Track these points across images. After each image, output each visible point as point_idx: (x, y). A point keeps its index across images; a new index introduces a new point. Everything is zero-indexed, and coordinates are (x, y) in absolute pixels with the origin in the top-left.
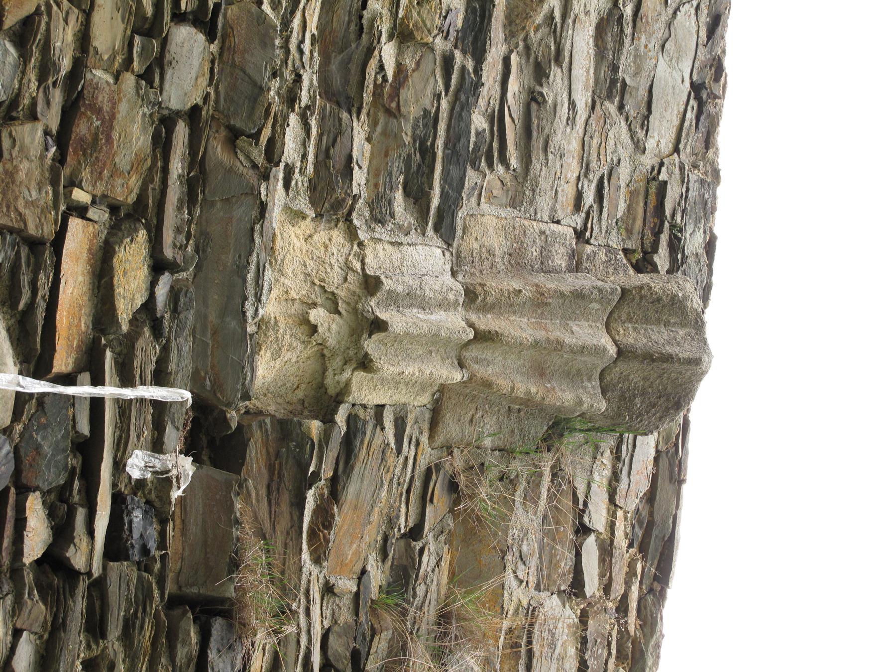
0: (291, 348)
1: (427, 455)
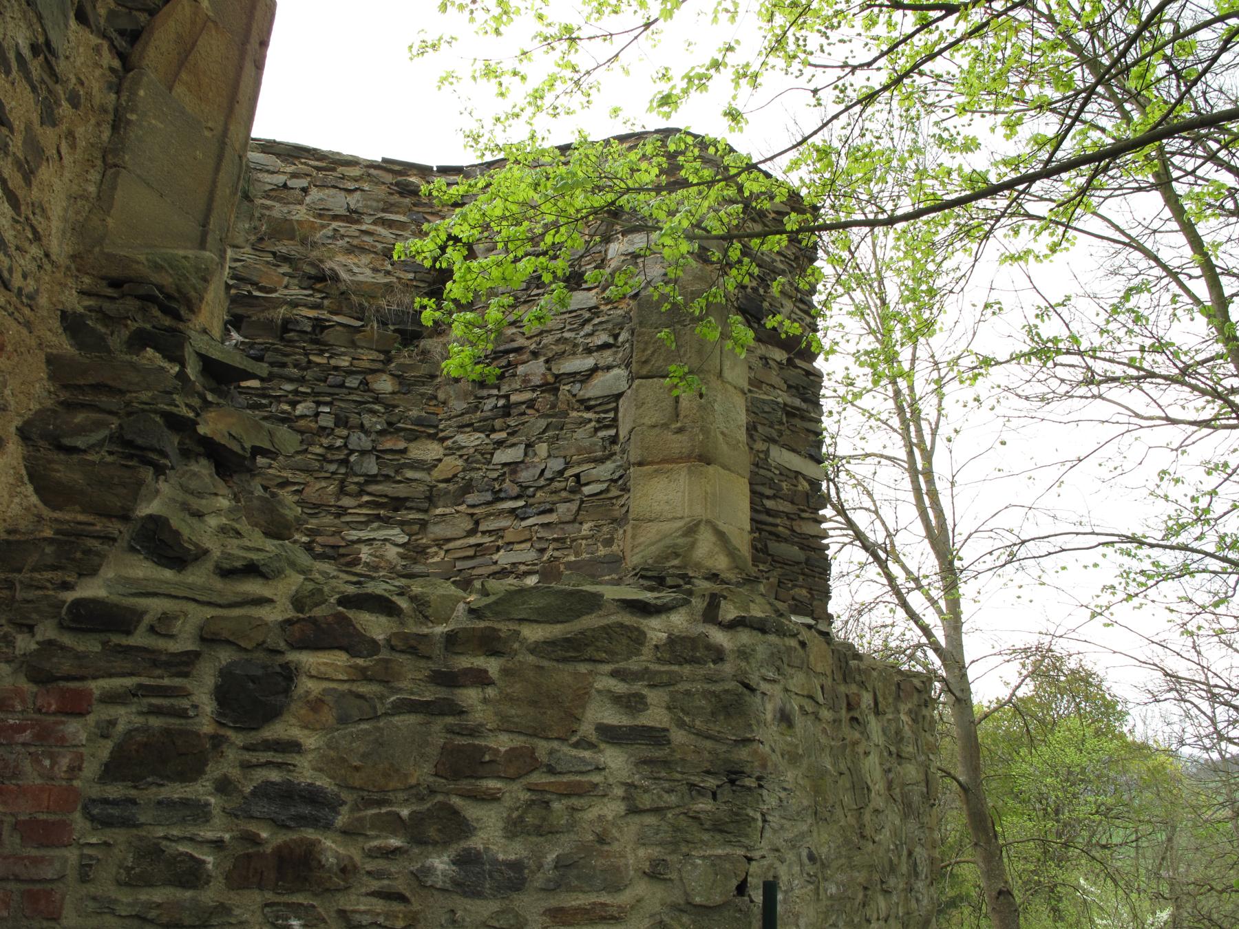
0: (666, 832)
1: (248, 249)
